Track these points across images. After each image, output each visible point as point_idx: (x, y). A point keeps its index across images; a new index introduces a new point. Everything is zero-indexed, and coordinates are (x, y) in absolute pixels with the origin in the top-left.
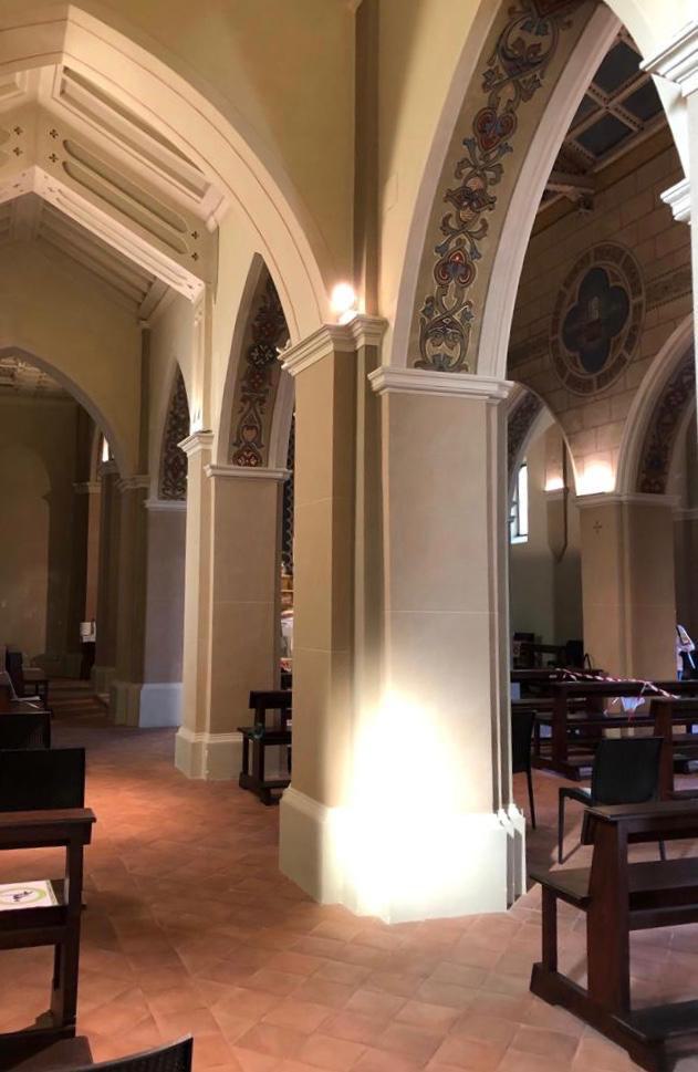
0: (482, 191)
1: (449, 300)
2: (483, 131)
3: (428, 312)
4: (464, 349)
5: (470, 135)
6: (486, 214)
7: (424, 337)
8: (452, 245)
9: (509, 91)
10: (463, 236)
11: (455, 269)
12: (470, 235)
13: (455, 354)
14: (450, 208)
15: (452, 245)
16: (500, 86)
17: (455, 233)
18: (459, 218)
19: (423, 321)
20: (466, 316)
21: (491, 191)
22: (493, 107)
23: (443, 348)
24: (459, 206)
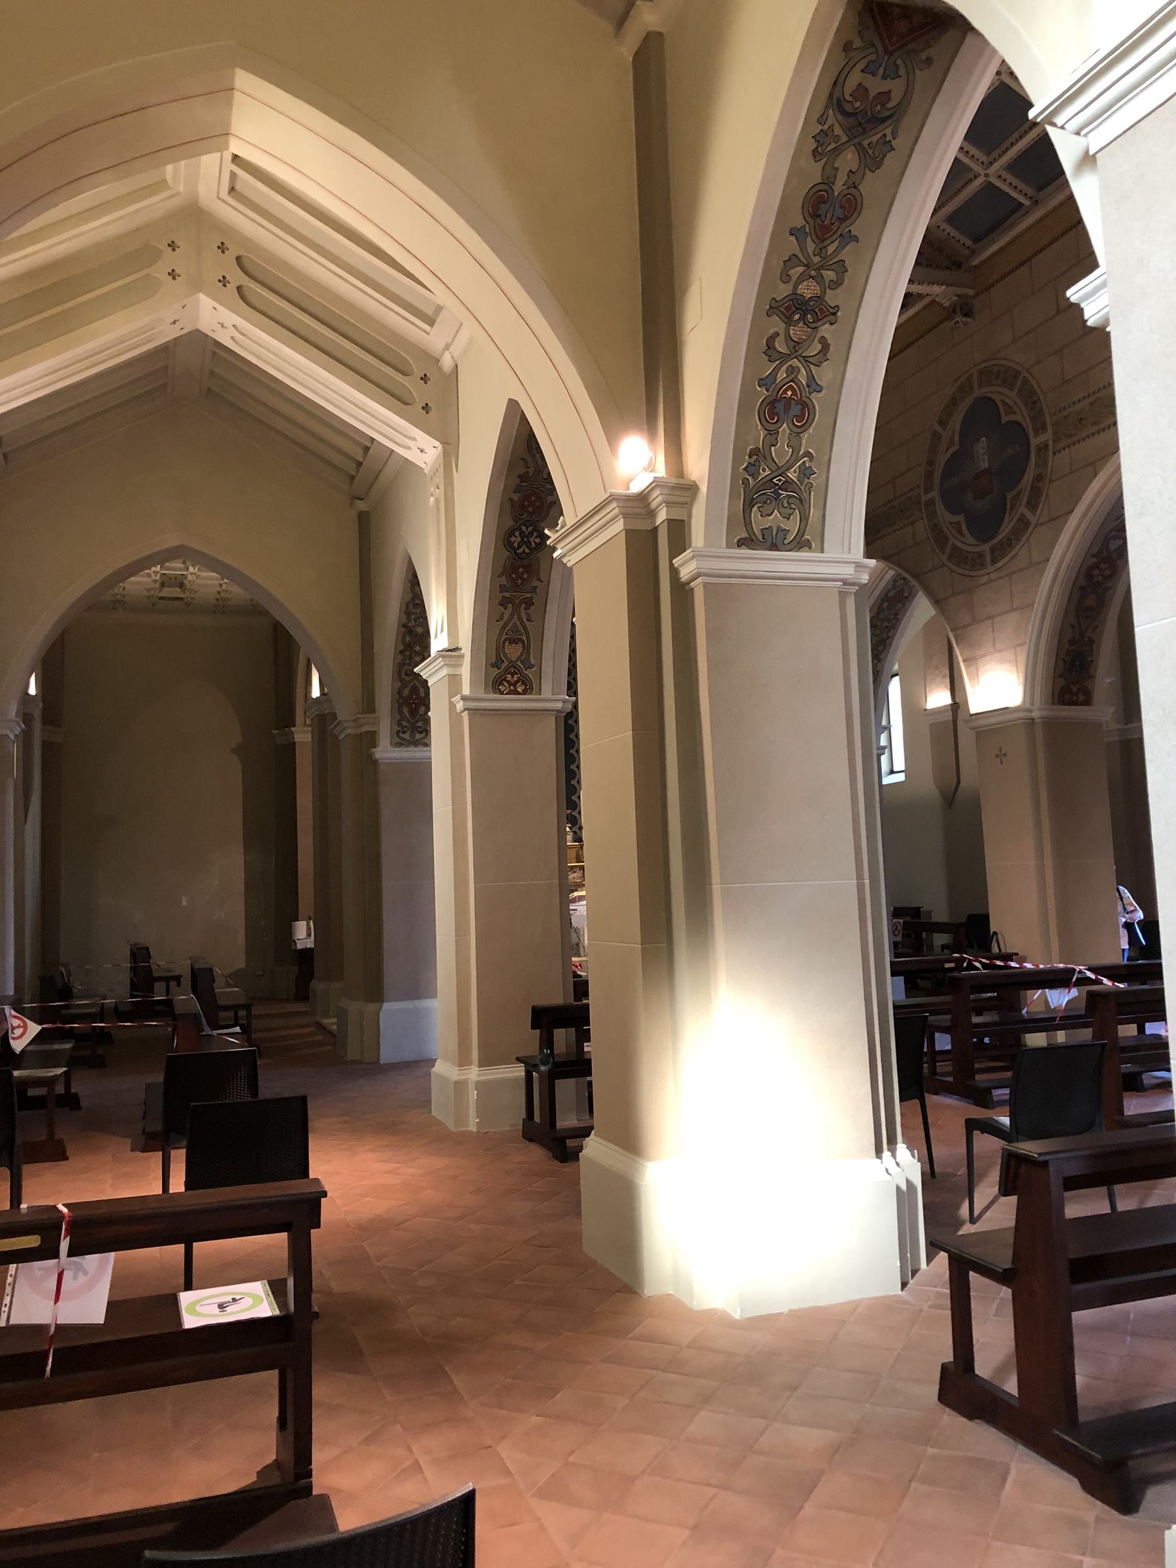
0: (820, 299)
1: (781, 452)
2: (815, 216)
3: (752, 469)
4: (804, 519)
5: (799, 222)
6: (825, 330)
7: (749, 504)
8: (782, 375)
9: (849, 159)
10: (795, 362)
11: (787, 408)
12: (806, 360)
13: (793, 526)
14: (776, 324)
15: (782, 375)
16: (837, 151)
17: (784, 358)
18: (788, 337)
19: (745, 482)
20: (806, 473)
21: (831, 298)
22: (828, 182)
23: (775, 519)
24: (788, 321)
